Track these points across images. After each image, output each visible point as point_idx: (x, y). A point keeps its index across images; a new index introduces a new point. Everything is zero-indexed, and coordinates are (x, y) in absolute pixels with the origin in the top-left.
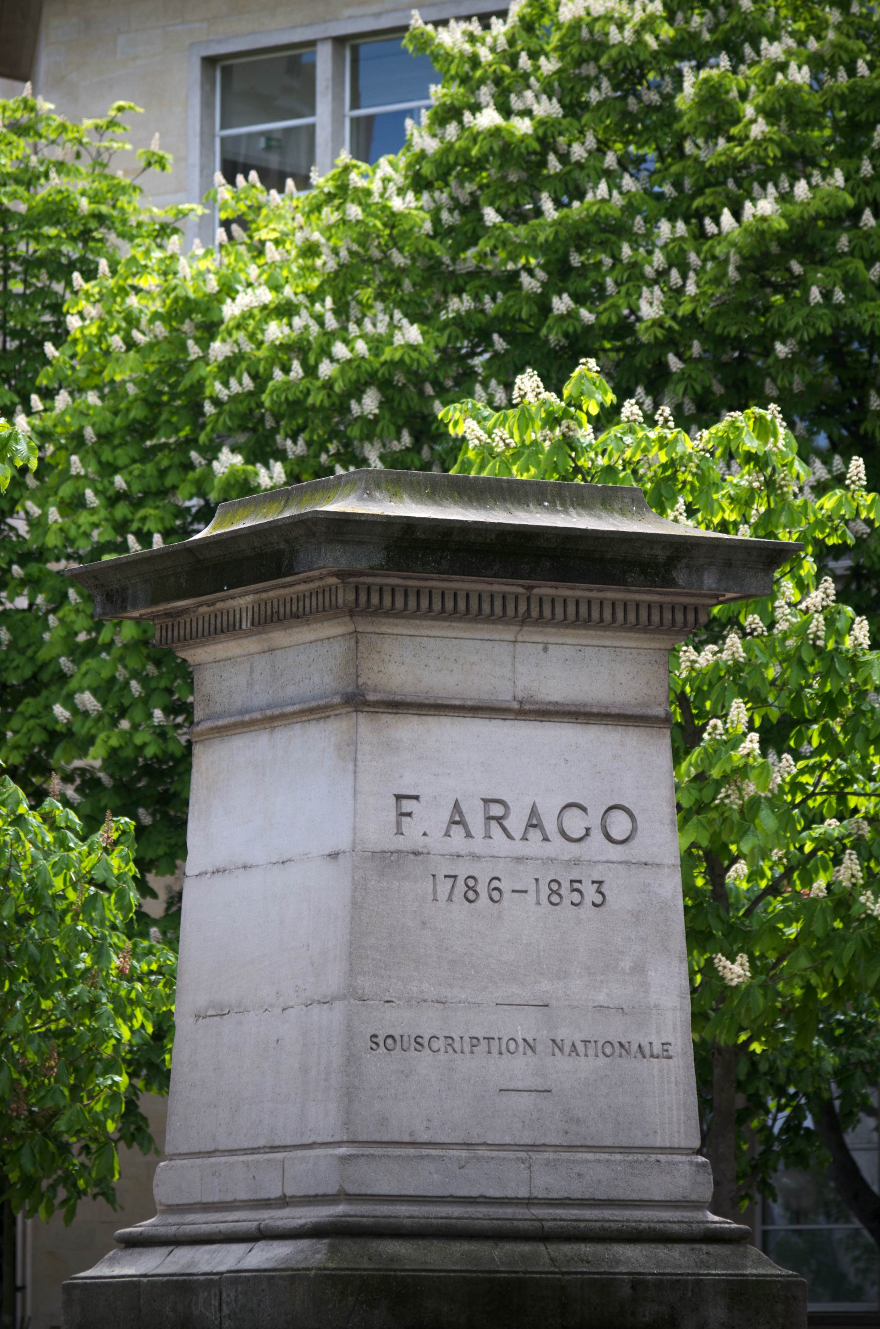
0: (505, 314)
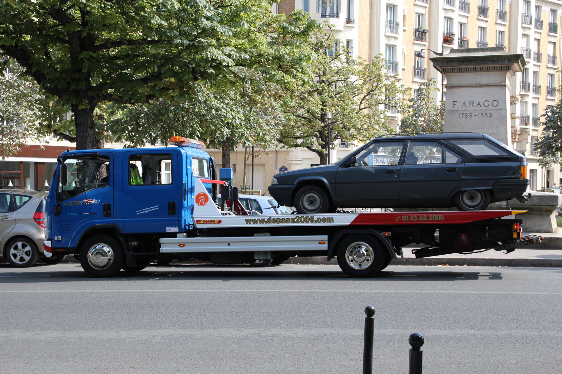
0: (27, 73)
